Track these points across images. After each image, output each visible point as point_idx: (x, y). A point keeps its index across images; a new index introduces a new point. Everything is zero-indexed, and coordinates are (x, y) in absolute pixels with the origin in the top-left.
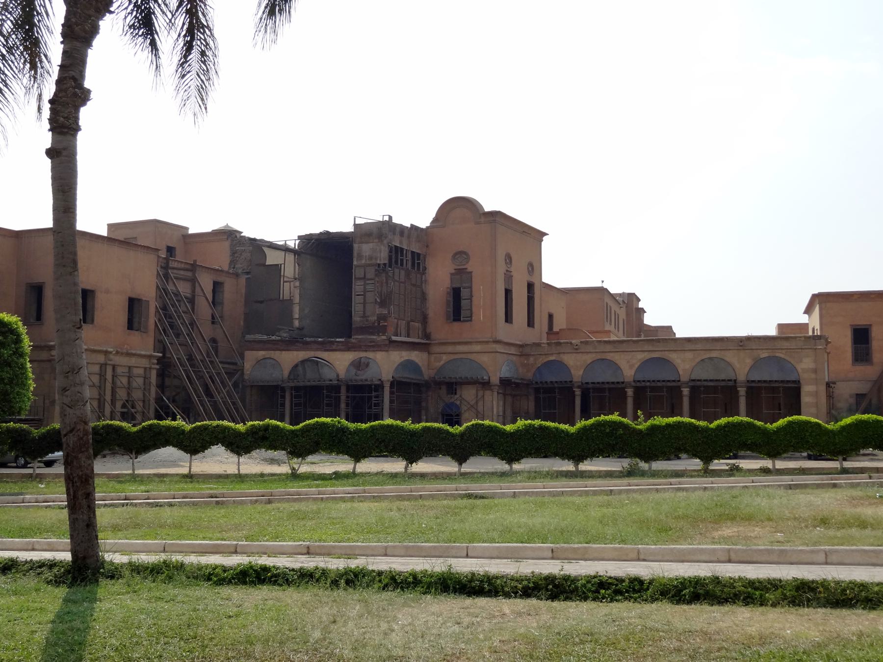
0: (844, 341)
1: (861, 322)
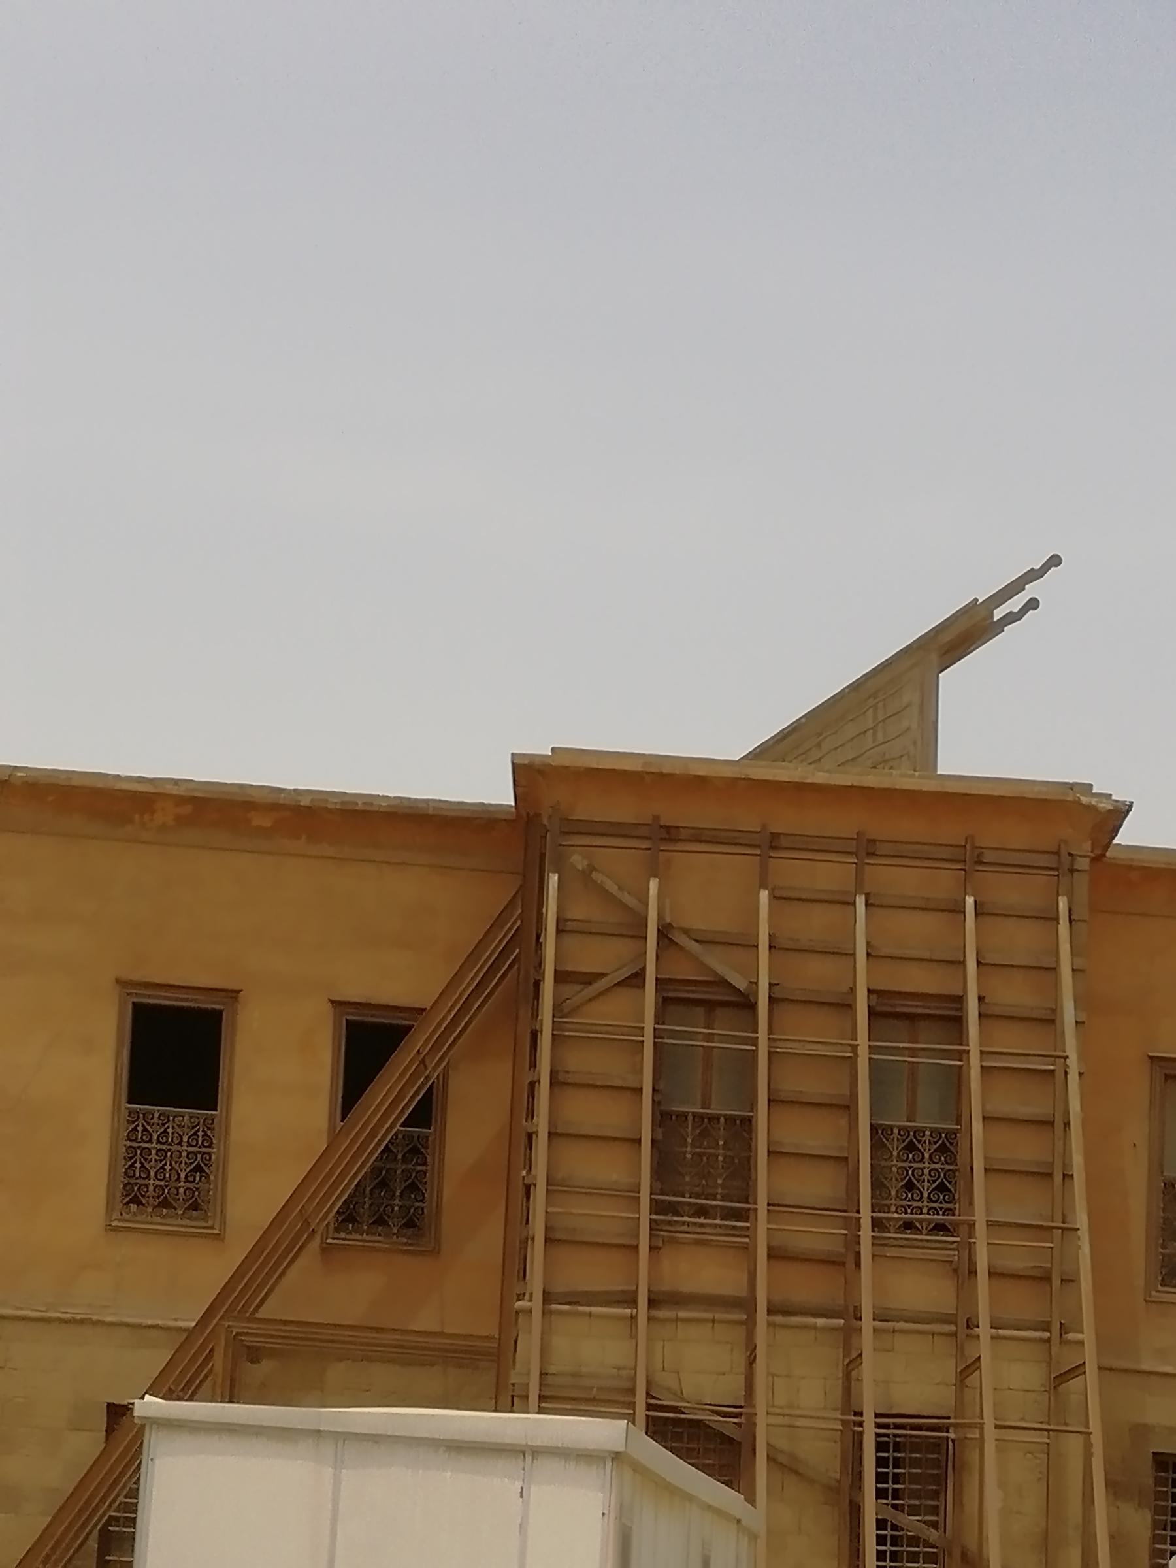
1: (183, 969)
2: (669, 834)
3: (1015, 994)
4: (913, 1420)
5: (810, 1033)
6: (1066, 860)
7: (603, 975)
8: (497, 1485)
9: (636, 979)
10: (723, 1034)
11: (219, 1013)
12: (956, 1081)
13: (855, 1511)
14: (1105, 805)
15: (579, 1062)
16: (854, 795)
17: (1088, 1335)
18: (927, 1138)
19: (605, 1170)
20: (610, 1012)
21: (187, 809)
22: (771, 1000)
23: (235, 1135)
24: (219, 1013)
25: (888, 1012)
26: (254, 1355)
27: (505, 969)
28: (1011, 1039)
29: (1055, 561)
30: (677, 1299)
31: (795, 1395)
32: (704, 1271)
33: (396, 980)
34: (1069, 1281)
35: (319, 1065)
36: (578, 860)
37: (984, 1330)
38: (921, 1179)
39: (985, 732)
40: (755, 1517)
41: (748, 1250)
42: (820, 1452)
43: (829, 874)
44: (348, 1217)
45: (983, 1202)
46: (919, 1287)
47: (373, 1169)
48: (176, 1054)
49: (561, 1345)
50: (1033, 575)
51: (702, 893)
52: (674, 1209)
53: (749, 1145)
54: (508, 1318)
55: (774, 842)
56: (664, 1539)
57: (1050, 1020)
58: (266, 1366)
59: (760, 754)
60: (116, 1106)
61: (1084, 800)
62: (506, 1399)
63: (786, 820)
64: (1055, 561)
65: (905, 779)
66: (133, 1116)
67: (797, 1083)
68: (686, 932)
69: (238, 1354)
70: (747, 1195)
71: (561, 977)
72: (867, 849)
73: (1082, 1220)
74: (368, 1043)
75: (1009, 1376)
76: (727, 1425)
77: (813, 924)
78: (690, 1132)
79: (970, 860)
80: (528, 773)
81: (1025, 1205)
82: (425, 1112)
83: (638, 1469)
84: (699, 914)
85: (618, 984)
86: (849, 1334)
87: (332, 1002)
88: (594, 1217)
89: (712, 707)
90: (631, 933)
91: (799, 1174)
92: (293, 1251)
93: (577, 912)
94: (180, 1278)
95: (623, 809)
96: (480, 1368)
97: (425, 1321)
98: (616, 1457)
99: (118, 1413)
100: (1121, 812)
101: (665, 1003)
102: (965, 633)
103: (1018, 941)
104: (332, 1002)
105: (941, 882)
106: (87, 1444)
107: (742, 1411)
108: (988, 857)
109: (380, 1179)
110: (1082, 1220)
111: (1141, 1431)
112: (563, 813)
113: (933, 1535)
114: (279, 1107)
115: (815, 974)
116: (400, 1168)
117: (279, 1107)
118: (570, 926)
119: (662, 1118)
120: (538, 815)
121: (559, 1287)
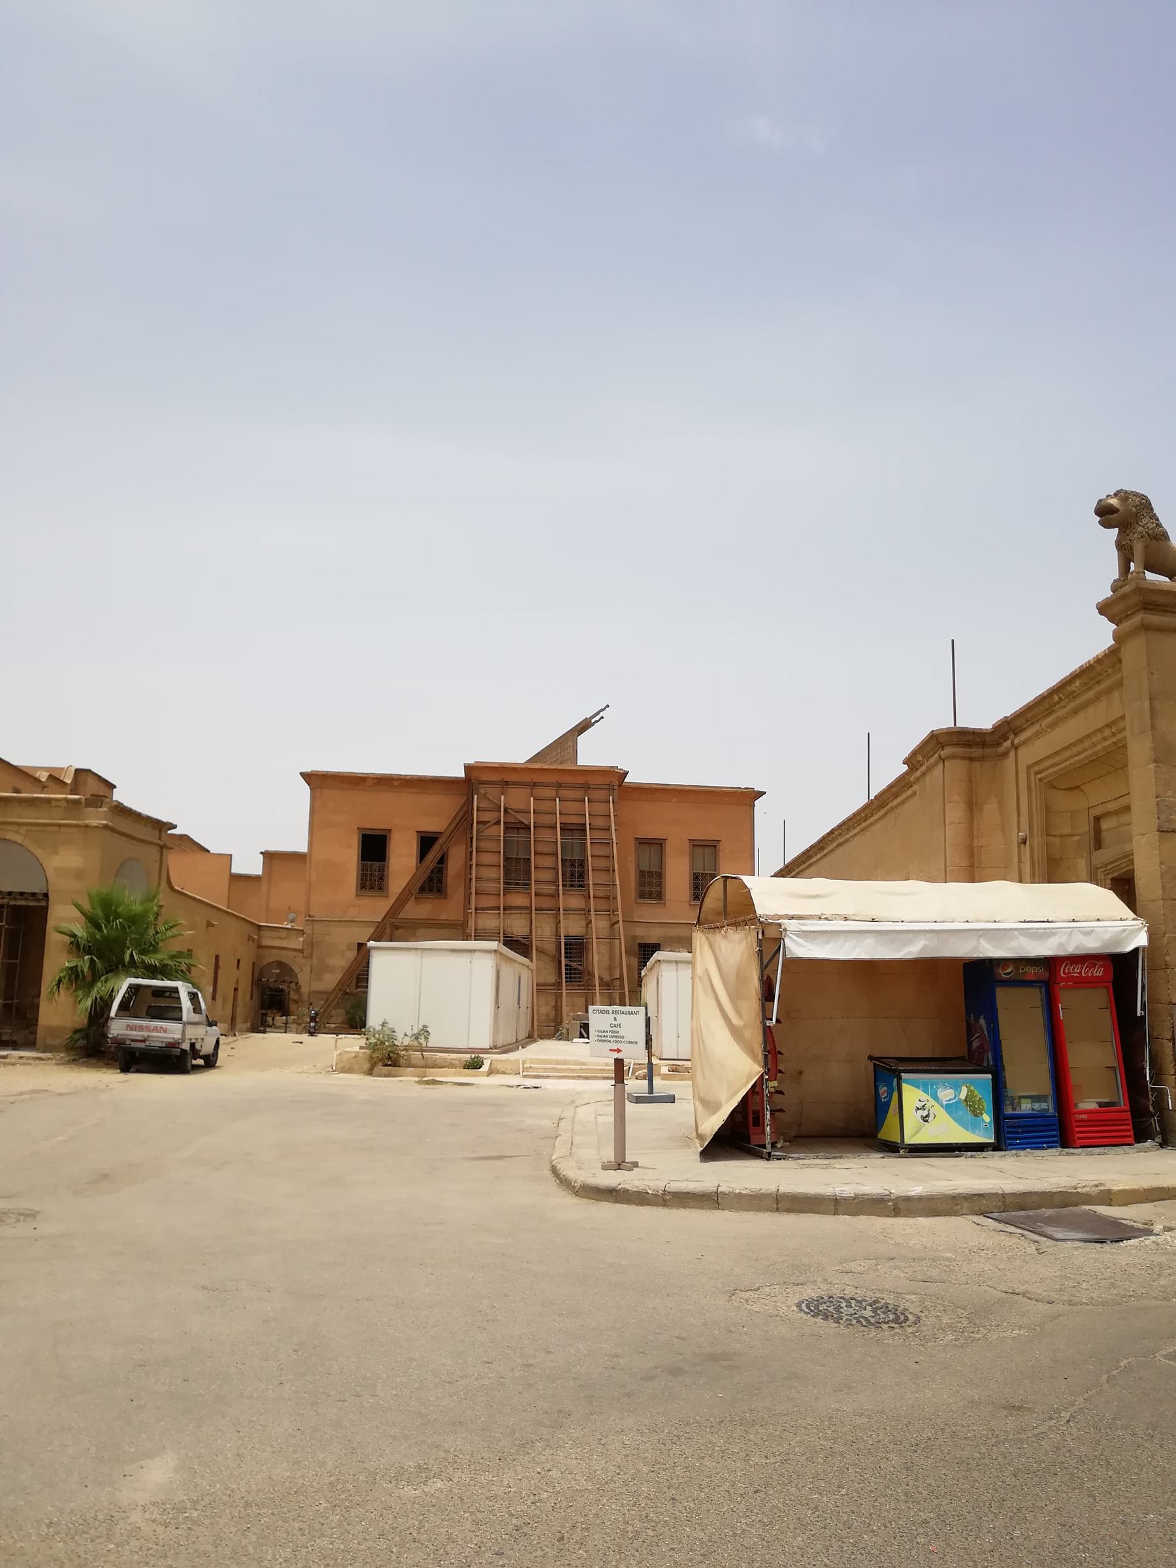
0: (350, 855)
1: (376, 823)
2: (507, 783)
3: (599, 822)
4: (576, 938)
5: (545, 835)
8: (464, 959)
10: (522, 836)
11: (385, 837)
12: (584, 846)
13: (560, 962)
15: (484, 845)
16: (556, 772)
17: (620, 913)
19: (492, 874)
20: (491, 831)
25: (565, 828)
26: (397, 928)
27: (463, 822)
28: (599, 835)
29: (217, 957)
30: (511, 908)
31: (543, 931)
32: (519, 900)
33: (434, 824)
34: (615, 898)
35: (413, 849)
36: (482, 791)
37: (592, 912)
38: (575, 874)
39: (591, 753)
40: (533, 965)
41: (530, 894)
42: (550, 947)
43: (549, 792)
44: (422, 890)
46: (576, 902)
48: (374, 847)
49: (480, 921)
50: (602, 710)
51: (515, 799)
52: (510, 884)
53: (530, 866)
54: (466, 915)
55: (535, 784)
56: (508, 972)
57: (608, 829)
58: (400, 931)
59: (529, 761)
62: (466, 937)
63: (537, 778)
64: (217, 957)
65: (568, 766)
66: (363, 865)
67: (542, 848)
69: (394, 929)
70: (530, 880)
71: (478, 822)
72: (560, 785)
73: (618, 882)
74: (427, 842)
75: (599, 925)
76: (524, 941)
77: (545, 806)
78: (513, 862)
79: (586, 787)
80: (468, 768)
81: (603, 878)
82: (442, 860)
83: (501, 954)
84: (514, 805)
86: (558, 915)
88: (490, 887)
89: (516, 748)
90: (274, 951)
91: (544, 872)
92: (407, 900)
93: (482, 805)
94: (377, 908)
96: (459, 929)
97: (443, 917)
98: (495, 951)
99: (361, 946)
100: (626, 773)
101: (506, 829)
102: (584, 726)
103: (600, 808)
105: (579, 794)
106: (352, 955)
107: (528, 937)
109: (430, 879)
110: (618, 882)
111: (634, 937)
112: (477, 779)
114: (403, 861)
115: (546, 819)
117: (403, 861)
119: (506, 859)
121: (479, 906)
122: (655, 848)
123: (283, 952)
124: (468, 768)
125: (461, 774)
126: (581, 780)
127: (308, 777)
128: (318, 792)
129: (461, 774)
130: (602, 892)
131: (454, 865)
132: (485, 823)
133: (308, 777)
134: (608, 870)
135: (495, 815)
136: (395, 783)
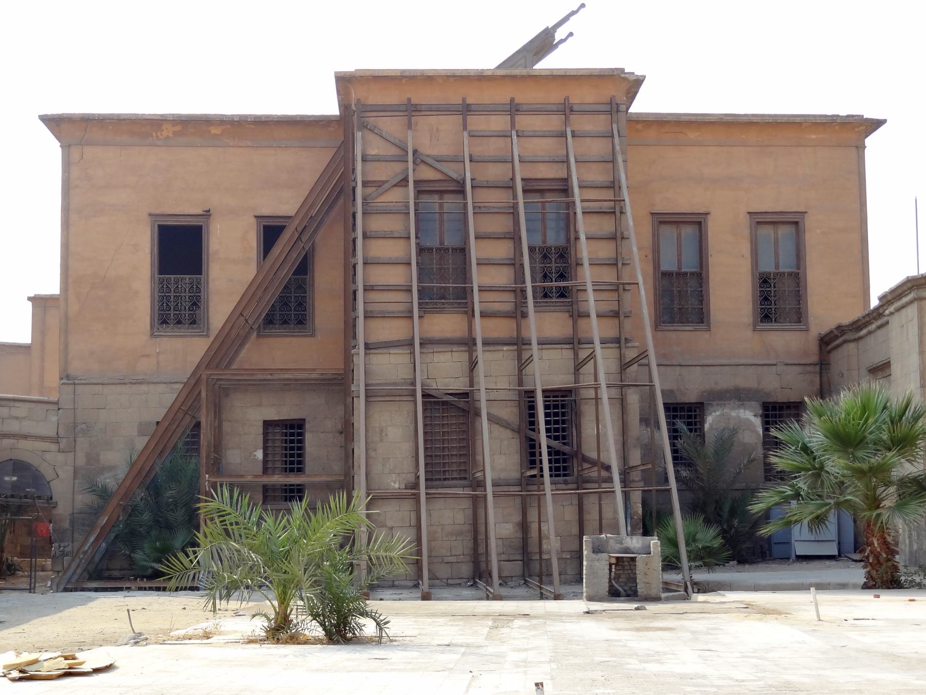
1: (182, 206)
6: (615, 106)
7: (387, 181)
9: (404, 182)
11: (200, 228)
14: (632, 78)
18: (553, 251)
21: (178, 128)
22: (472, 187)
23: (211, 285)
24: (200, 228)
25: (532, 188)
29: (583, 6)
32: (447, 324)
33: (285, 203)
44: (269, 321)
45: (587, 275)
47: (280, 297)
48: (180, 248)
51: (437, 137)
54: (348, 359)
60: (152, 277)
61: (623, 75)
64: (583, 6)
66: (161, 282)
68: (428, 156)
71: (365, 184)
72: (514, 109)
74: (270, 232)
76: (461, 403)
80: (346, 83)
82: (304, 268)
85: (395, 186)
87: (256, 217)
93: (373, 151)
95: (392, 97)
100: (633, 85)
101: (419, 193)
104: (256, 217)
108: (575, 108)
113: (566, 449)
116: (293, 295)
118: (409, 398)
119: (421, 250)
120: (351, 105)
121: (373, 339)
122: (688, 231)
123: (23, 444)
124: (346, 83)
125: (330, 107)
126: (555, 96)
127: (56, 124)
128: (75, 153)
129: (330, 107)
130: (608, 275)
131: (326, 279)
132: (379, 184)
133: (56, 124)
134: (617, 237)
135: (398, 167)
136: (215, 130)
